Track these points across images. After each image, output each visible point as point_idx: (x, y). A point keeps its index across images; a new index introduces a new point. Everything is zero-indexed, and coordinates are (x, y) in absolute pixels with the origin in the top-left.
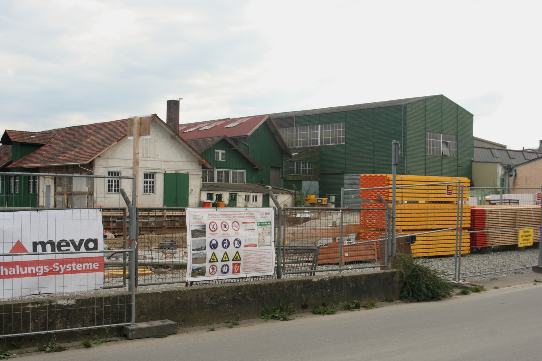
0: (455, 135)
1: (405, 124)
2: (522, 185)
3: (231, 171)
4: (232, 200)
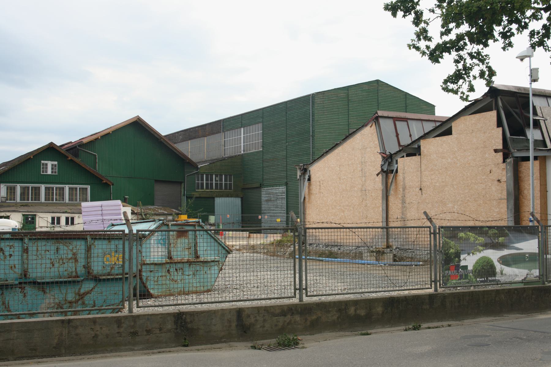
2: (316, 194)
3: (67, 188)
4: (27, 223)
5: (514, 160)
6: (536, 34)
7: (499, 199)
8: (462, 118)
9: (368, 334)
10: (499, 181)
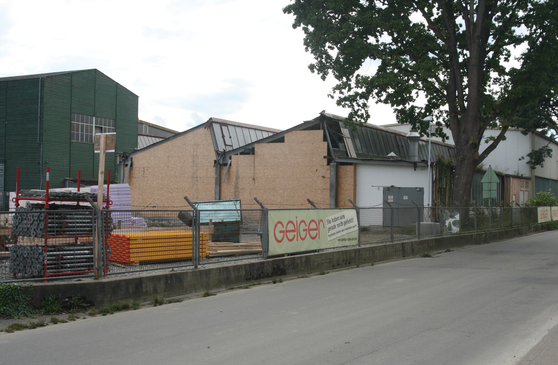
0: (113, 119)
1: (42, 102)
2: (139, 178)
5: (336, 164)
6: (400, 107)
7: (323, 189)
8: (294, 132)
9: (178, 301)
10: (323, 177)
